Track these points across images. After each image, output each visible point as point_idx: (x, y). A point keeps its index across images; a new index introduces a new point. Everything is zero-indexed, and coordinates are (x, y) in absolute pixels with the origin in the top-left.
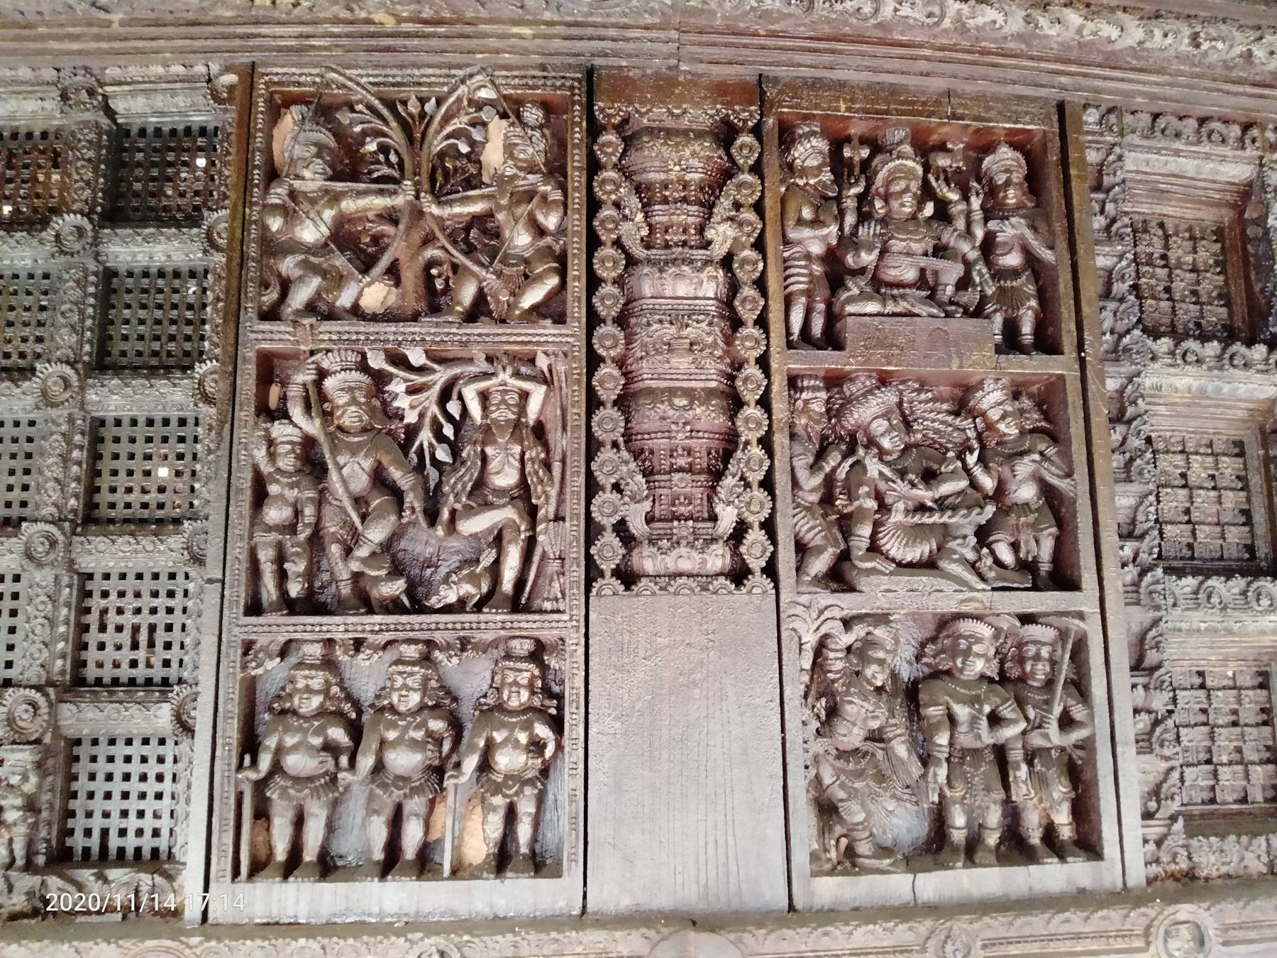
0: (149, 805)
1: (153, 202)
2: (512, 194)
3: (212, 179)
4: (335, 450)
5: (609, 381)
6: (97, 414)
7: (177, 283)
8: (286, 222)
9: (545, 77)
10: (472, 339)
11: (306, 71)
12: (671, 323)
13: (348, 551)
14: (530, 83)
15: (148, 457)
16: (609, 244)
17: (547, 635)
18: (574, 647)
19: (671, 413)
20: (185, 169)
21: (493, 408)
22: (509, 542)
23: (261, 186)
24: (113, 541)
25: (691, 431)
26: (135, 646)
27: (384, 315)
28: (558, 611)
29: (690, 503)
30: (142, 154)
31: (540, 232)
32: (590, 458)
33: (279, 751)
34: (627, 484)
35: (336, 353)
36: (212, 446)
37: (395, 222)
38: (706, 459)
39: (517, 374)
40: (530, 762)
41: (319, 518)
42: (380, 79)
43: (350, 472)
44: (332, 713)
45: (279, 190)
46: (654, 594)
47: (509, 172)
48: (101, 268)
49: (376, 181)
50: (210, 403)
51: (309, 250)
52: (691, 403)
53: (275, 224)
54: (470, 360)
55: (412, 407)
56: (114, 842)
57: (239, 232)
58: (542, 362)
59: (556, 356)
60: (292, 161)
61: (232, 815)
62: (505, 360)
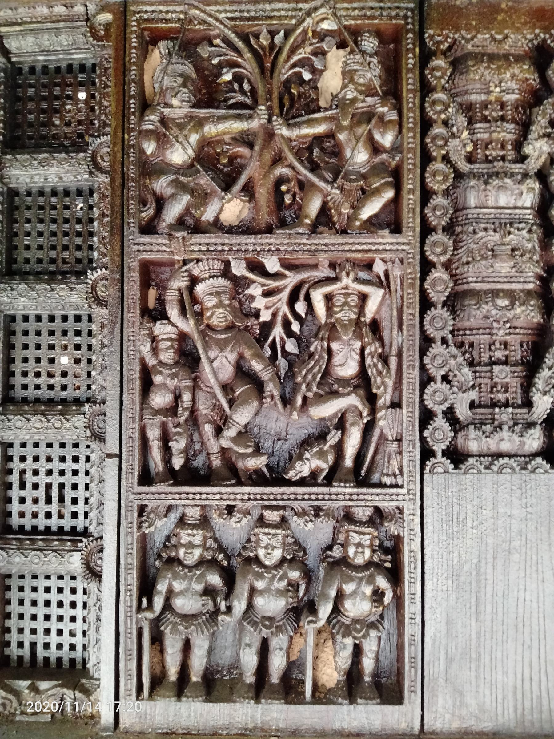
0: (66, 626)
1: (44, 131)
2: (353, 115)
3: (92, 109)
4: (206, 347)
5: (439, 284)
6: (8, 313)
7: (67, 201)
8: (158, 147)
9: (381, 8)
10: (320, 248)
11: (171, 8)
12: (495, 231)
13: (219, 431)
14: (369, 13)
15: (52, 347)
16: (439, 159)
17: (387, 505)
18: (411, 517)
19: (494, 312)
20: (69, 102)
21: (336, 309)
22: (352, 424)
23: (137, 114)
24: (28, 420)
25: (510, 328)
26: (49, 501)
27: (239, 227)
28: (396, 486)
29: (506, 391)
30: (33, 90)
31: (375, 149)
32: (423, 353)
33: (170, 594)
34: (455, 376)
35: (205, 261)
36: (106, 342)
37: (251, 146)
38: (520, 352)
39: (357, 280)
40: (374, 610)
41: (194, 401)
42: (237, 14)
43: (219, 365)
44: (209, 561)
45: (152, 117)
46: (479, 472)
47: (350, 96)
48: (5, 188)
49: (231, 107)
50: (102, 305)
51: (179, 170)
52: (512, 304)
53: (150, 147)
54: (315, 266)
55: (267, 308)
56: (41, 653)
57: (119, 155)
58: (379, 268)
59: (393, 262)
60: (162, 92)
61: (135, 648)
62: (348, 266)
